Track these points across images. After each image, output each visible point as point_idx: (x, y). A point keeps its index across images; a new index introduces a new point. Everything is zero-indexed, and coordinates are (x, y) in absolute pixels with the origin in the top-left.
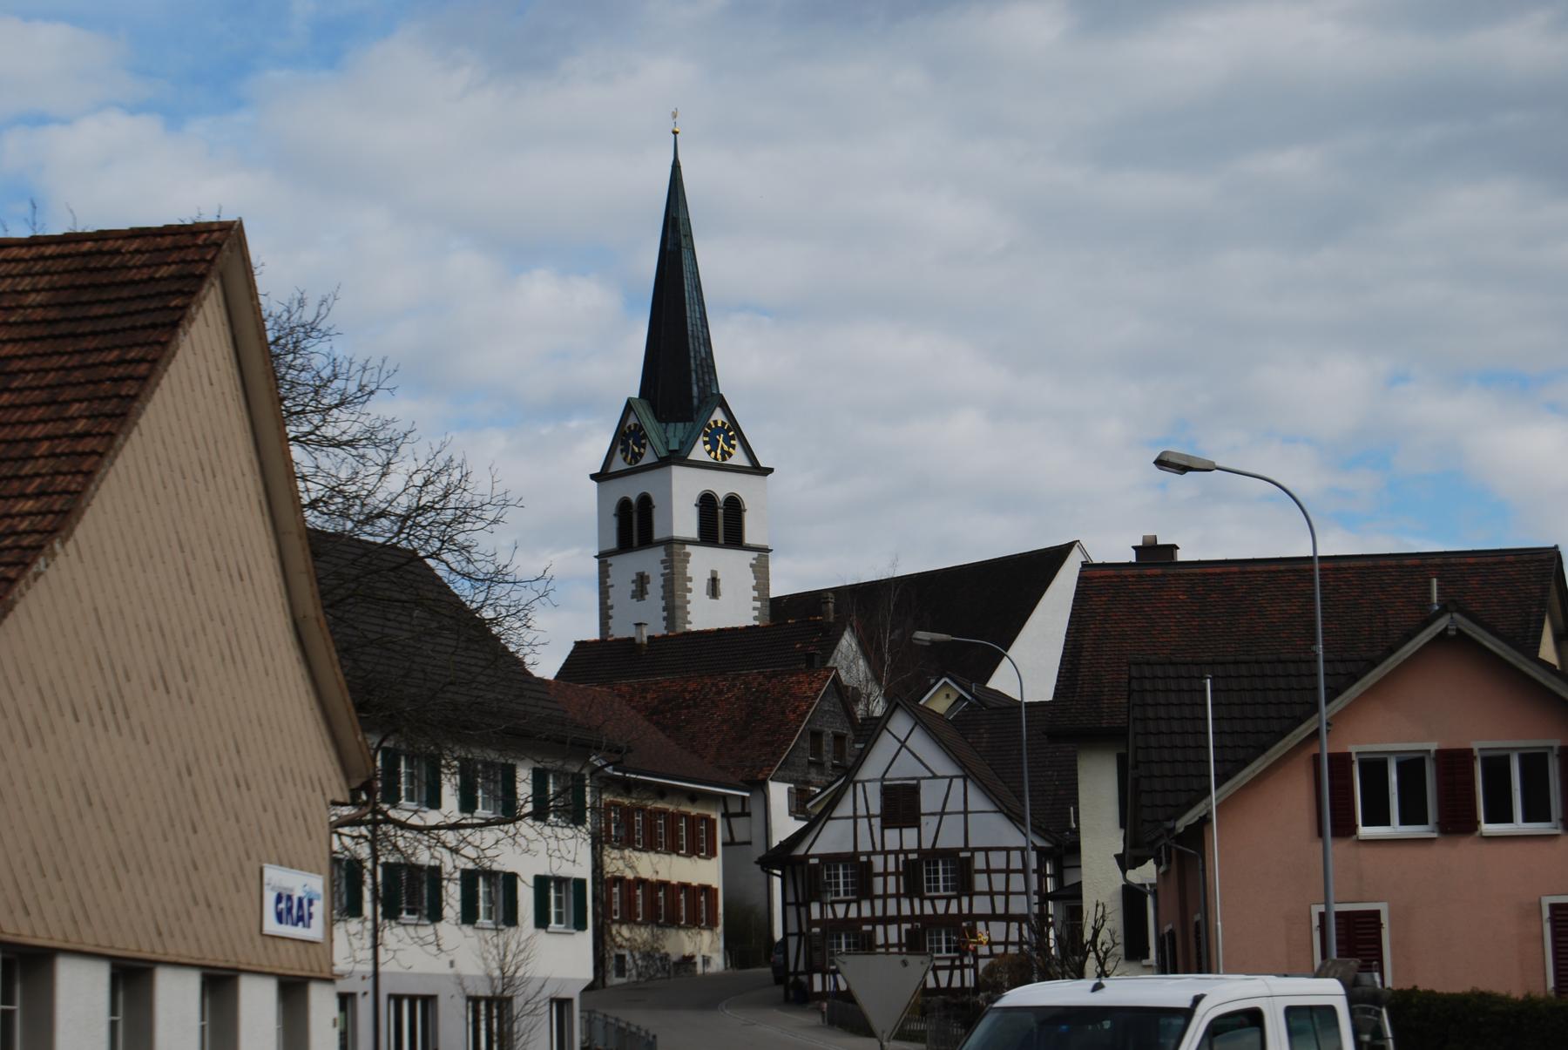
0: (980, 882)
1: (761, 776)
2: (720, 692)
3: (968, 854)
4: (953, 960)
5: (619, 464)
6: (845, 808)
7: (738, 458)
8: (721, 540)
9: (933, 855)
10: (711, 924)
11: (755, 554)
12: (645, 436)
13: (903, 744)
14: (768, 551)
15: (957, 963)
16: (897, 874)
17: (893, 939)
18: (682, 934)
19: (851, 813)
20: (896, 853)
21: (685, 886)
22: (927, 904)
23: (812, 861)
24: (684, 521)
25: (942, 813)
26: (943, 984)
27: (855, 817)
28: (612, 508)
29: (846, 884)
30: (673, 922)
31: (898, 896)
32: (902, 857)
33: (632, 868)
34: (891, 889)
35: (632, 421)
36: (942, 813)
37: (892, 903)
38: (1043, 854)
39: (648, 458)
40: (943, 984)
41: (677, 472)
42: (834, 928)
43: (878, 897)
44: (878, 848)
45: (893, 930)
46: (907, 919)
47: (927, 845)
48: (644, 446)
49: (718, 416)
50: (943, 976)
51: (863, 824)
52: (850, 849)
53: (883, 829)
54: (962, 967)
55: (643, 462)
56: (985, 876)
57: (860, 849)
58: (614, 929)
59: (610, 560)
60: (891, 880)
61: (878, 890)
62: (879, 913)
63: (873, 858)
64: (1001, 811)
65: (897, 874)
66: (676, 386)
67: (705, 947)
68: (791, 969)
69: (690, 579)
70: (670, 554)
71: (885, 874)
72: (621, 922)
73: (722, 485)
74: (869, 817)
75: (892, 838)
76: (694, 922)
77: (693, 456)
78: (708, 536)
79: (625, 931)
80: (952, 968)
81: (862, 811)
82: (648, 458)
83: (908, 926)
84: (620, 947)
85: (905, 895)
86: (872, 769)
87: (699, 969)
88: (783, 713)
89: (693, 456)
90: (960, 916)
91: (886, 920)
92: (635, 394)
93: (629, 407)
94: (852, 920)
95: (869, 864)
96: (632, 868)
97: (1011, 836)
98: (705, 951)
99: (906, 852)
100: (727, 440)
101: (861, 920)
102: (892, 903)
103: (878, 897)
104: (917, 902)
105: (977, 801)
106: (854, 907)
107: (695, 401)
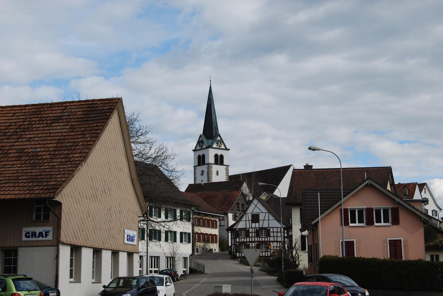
0: (272, 234)
2: (218, 195)
6: (244, 219)
7: (223, 147)
9: (262, 229)
10: (216, 242)
13: (256, 206)
14: (228, 166)
16: (254, 232)
17: (254, 246)
18: (210, 244)
20: (254, 228)
21: (211, 234)
22: (261, 239)
24: (211, 160)
25: (264, 220)
26: (264, 255)
27: (246, 221)
28: (197, 157)
30: (208, 242)
31: (255, 237)
34: (253, 236)
35: (201, 139)
36: (264, 220)
37: (253, 238)
38: (284, 229)
39: (204, 147)
41: (210, 149)
42: (242, 243)
45: (253, 244)
47: (261, 226)
49: (219, 138)
50: (264, 253)
51: (248, 222)
54: (268, 252)
58: (196, 243)
60: (253, 234)
61: (251, 236)
62: (251, 240)
65: (254, 232)
67: (215, 247)
70: (208, 166)
71: (252, 232)
72: (198, 242)
73: (219, 152)
74: (249, 221)
76: (213, 242)
78: (216, 163)
79: (198, 243)
80: (265, 252)
81: (247, 219)
82: (204, 147)
86: (250, 211)
87: (214, 252)
91: (252, 242)
93: (200, 136)
95: (249, 230)
99: (256, 228)
100: (221, 143)
101: (247, 242)
102: (253, 238)
105: (271, 217)
106: (245, 239)
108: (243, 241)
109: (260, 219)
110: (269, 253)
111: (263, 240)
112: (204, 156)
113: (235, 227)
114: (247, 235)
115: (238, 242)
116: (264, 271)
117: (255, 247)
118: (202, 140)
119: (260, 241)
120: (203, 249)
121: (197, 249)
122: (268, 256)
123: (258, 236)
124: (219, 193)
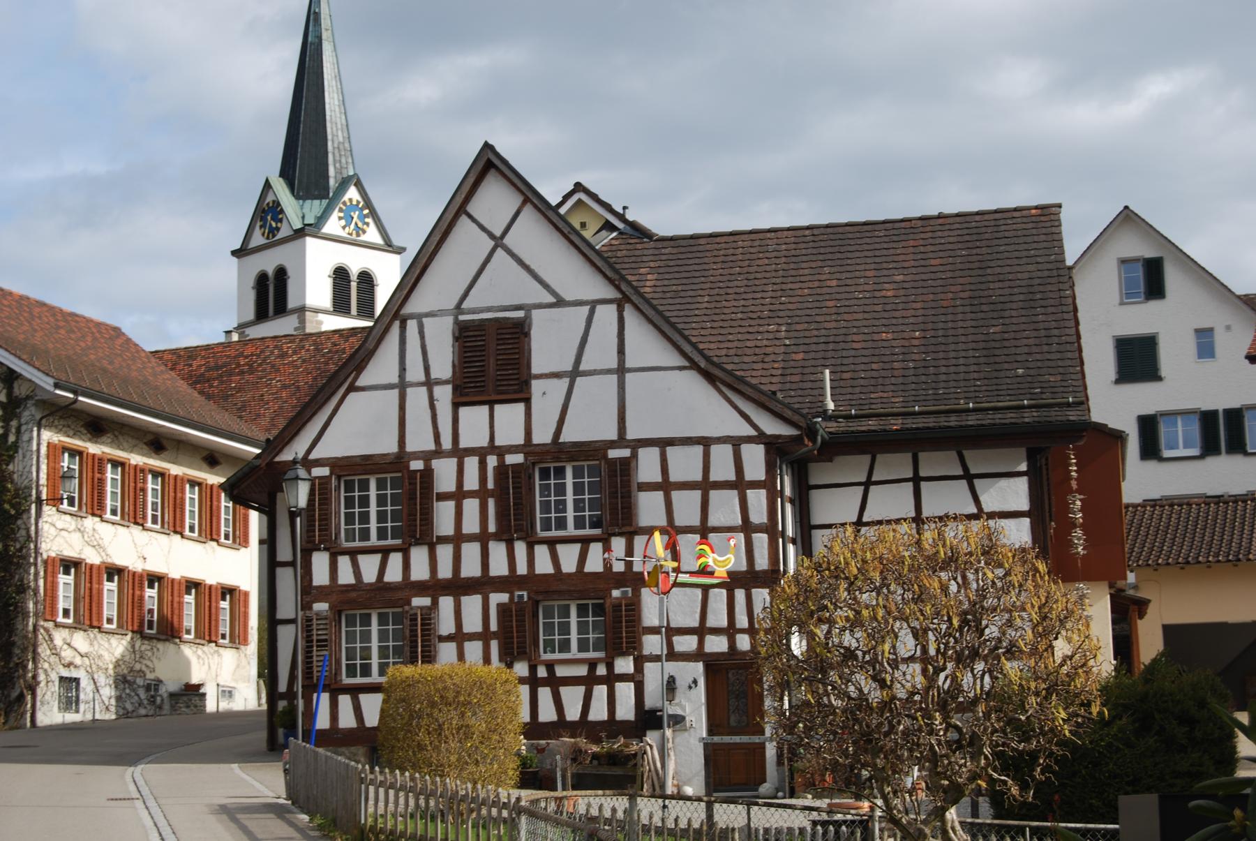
0: (649, 508)
2: (283, 355)
3: (626, 453)
4: (592, 665)
5: (258, 239)
7: (372, 235)
8: (354, 311)
9: (558, 454)
10: (237, 639)
12: (282, 211)
13: (499, 242)
15: (601, 670)
16: (482, 494)
17: (473, 623)
18: (187, 650)
19: (395, 380)
20: (481, 453)
21: (192, 585)
22: (542, 552)
25: (575, 373)
26: (573, 714)
27: (402, 386)
28: (251, 281)
29: (381, 517)
30: (168, 631)
31: (483, 538)
32: (492, 461)
33: (98, 547)
34: (471, 525)
35: (270, 198)
36: (575, 373)
37: (471, 552)
38: (776, 449)
40: (573, 714)
41: (310, 242)
42: (354, 602)
44: (447, 444)
45: (472, 604)
47: (542, 436)
48: (281, 221)
50: (572, 698)
51: (418, 398)
52: (391, 447)
53: (456, 405)
54: (611, 679)
55: (280, 236)
56: (659, 496)
57: (410, 448)
58: (59, 637)
60: (471, 506)
62: (445, 572)
63: (436, 464)
64: (694, 366)
65: (482, 494)
67: (228, 676)
71: (459, 495)
72: (75, 627)
73: (356, 261)
74: (429, 383)
75: (474, 425)
76: (207, 633)
79: (80, 640)
80: (589, 681)
81: (415, 372)
82: (284, 232)
83: (504, 597)
85: (497, 537)
87: (211, 706)
90: (608, 578)
91: (459, 587)
95: (428, 474)
96: (98, 547)
97: (714, 413)
98: (226, 680)
99: (501, 452)
101: (411, 587)
102: (471, 552)
103: (443, 540)
104: (520, 548)
105: (644, 345)
106: (396, 560)
108: (370, 576)
109: (535, 370)
110: (625, 691)
111: (569, 566)
112: (281, 273)
114: (414, 528)
117: (484, 636)
118: (277, 204)
119: (531, 580)
120: (123, 681)
121: (70, 684)
122: (612, 727)
123: (515, 522)
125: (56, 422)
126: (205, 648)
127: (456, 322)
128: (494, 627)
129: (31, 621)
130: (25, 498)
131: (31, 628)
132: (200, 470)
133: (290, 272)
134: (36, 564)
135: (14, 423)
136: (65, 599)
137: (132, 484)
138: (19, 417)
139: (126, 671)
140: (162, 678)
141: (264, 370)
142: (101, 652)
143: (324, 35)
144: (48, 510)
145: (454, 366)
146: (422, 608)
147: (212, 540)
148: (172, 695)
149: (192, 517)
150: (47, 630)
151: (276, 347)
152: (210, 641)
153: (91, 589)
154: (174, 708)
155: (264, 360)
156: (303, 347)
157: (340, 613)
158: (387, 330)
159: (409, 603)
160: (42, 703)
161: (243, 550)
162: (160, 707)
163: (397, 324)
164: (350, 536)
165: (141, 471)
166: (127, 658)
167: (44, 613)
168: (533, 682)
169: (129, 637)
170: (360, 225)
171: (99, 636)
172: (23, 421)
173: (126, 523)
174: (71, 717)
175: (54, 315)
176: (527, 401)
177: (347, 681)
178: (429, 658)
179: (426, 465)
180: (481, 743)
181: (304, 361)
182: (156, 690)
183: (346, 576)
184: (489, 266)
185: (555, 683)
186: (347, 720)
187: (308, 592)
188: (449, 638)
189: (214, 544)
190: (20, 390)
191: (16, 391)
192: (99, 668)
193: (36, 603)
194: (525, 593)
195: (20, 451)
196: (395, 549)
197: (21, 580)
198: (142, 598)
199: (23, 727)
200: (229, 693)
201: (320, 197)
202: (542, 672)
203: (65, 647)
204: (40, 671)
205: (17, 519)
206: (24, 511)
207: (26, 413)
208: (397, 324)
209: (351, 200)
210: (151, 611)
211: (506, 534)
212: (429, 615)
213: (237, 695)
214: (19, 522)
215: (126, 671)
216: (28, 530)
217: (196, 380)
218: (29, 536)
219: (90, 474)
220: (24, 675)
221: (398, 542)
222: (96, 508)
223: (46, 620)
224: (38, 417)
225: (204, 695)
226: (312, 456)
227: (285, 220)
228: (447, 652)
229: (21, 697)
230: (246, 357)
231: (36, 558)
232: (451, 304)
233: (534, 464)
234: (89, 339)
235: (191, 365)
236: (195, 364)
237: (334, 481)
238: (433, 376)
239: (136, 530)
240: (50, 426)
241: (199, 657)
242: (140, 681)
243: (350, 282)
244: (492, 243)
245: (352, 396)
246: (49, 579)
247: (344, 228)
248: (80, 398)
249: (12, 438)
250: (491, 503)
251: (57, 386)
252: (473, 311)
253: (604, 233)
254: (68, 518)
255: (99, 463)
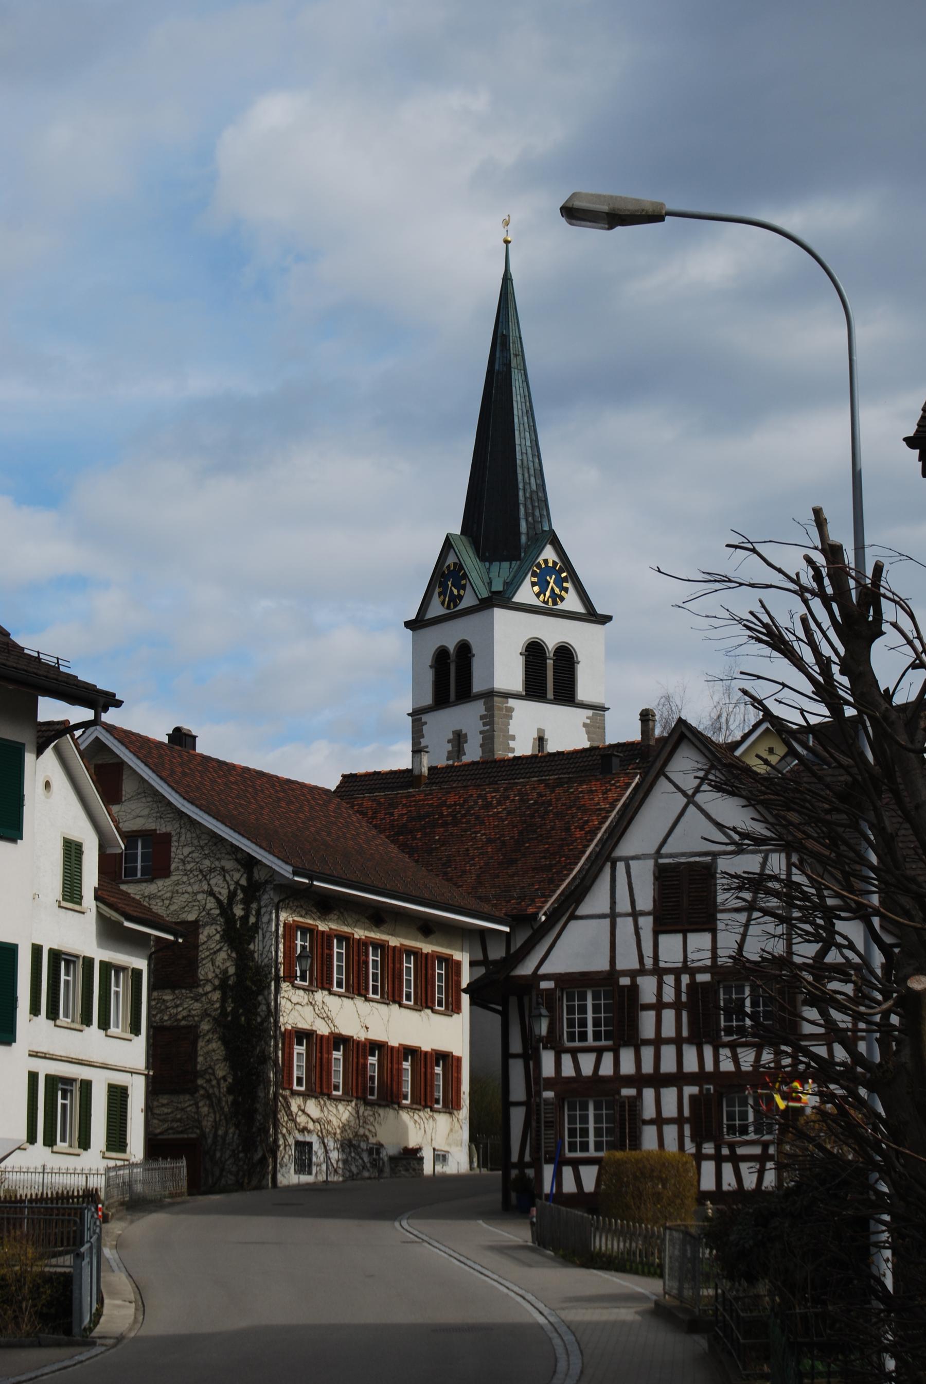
1: (531, 910)
2: (488, 806)
4: (765, 1146)
5: (436, 609)
6: (597, 901)
7: (571, 602)
8: (550, 695)
9: (741, 970)
10: (451, 1105)
11: (590, 713)
12: (465, 576)
14: (603, 709)
16: (677, 1006)
17: (670, 1110)
18: (405, 1116)
19: (607, 910)
20: (677, 973)
21: (410, 1052)
23: (544, 985)
24: (507, 671)
27: (613, 916)
28: (428, 659)
29: (596, 1023)
30: (390, 1098)
31: (678, 1042)
32: (685, 979)
33: (327, 1018)
34: (668, 1031)
35: (451, 560)
39: (469, 600)
41: (499, 614)
42: (577, 1090)
43: (647, 1042)
44: (649, 963)
45: (669, 1095)
46: (692, 1079)
48: (464, 587)
49: (549, 554)
51: (625, 926)
52: (606, 967)
53: (656, 933)
55: (463, 605)
57: (619, 967)
58: (295, 1103)
59: (425, 718)
60: (669, 1016)
61: (647, 1028)
63: (640, 980)
65: (677, 1006)
66: (505, 519)
67: (442, 1139)
68: (515, 1158)
69: (513, 738)
70: (490, 708)
71: (659, 1006)
72: (306, 1095)
73: (552, 632)
74: (635, 914)
75: (671, 948)
76: (424, 1100)
77: (519, 598)
78: (534, 690)
79: (312, 1107)
81: (623, 905)
82: (469, 600)
83: (694, 1090)
84: (304, 1130)
85: (690, 1041)
86: (641, 839)
87: (428, 1168)
88: (568, 830)
89: (519, 598)
91: (659, 1080)
92: (457, 530)
93: (448, 544)
94: (605, 1079)
95: (634, 989)
96: (327, 1018)
98: (441, 1144)
99: (693, 972)
100: (559, 582)
101: (619, 1080)
103: (647, 1042)
104: (708, 1051)
106: (608, 1058)
107: (523, 539)
108: (750, 1182)
112: (464, 649)
113: (526, 969)
114: (622, 1029)
115: (550, 1083)
116: (693, 1326)
117: (679, 1121)
118: (459, 566)
119: (717, 1076)
120: (349, 1145)
121: (304, 1148)
123: (702, 1032)
124: (492, 796)
125: (291, 904)
126: (421, 1114)
127: (657, 865)
128: (686, 1113)
129: (272, 1090)
130: (266, 976)
131: (271, 1096)
132: (416, 940)
133: (475, 650)
134: (275, 1037)
135: (254, 905)
136: (298, 1069)
137: (356, 958)
138: (259, 901)
139: (351, 1136)
140: (383, 1142)
141: (468, 822)
142: (330, 1118)
143: (513, 364)
144: (285, 986)
145: (654, 901)
146: (628, 1097)
147: (427, 1007)
148: (392, 1159)
149: (409, 986)
150: (285, 1098)
151: (480, 796)
152: (426, 1106)
153: (321, 1059)
154: (393, 1171)
155: (468, 811)
156: (508, 797)
157: (563, 1100)
158: (600, 870)
159: (619, 1093)
160: (281, 1166)
161: (455, 1016)
162: (381, 1171)
163: (609, 864)
164: (571, 1038)
165: (364, 944)
166: (352, 1124)
167: (282, 1082)
168: (719, 1159)
169: (353, 1104)
170: (557, 591)
171: (328, 1103)
172: (262, 903)
173: (351, 995)
174: (305, 1179)
175: (273, 786)
176: (714, 931)
177: (569, 1155)
178: (636, 1142)
179: (632, 981)
180: (669, 1205)
181: (509, 813)
182: (378, 1153)
183: (568, 1070)
184: (683, 820)
185: (736, 1160)
186: (569, 1186)
187: (534, 1080)
188: (651, 1122)
189: (429, 1011)
190: (259, 875)
191: (256, 876)
192: (328, 1132)
193: (275, 1074)
194: (712, 1087)
195: (260, 932)
196: (607, 1049)
197: (263, 1051)
198: (365, 1065)
199: (266, 1187)
200: (440, 1157)
201: (510, 559)
202: (725, 1151)
203: (300, 1113)
204: (280, 1136)
205: (258, 995)
206: (264, 988)
207: (266, 897)
208: (609, 864)
209: (546, 561)
210: (372, 1078)
211: (697, 1040)
212: (636, 1103)
213: (450, 1159)
214: (260, 998)
215: (351, 1136)
216: (269, 1005)
217: (399, 834)
218: (269, 1010)
219: (320, 950)
220: (267, 1139)
221: (610, 1043)
222: (324, 983)
223: (284, 1089)
224: (276, 900)
225: (422, 1159)
226: (542, 971)
227: (468, 587)
228: (649, 1136)
229: (263, 1160)
230: (450, 807)
231: (275, 1032)
232: (652, 850)
233: (719, 982)
234: (306, 808)
235: (392, 814)
236: (396, 813)
237: (558, 993)
238: (638, 909)
239: (359, 1001)
240: (286, 908)
241: (415, 1122)
242: (363, 1145)
243: (545, 659)
244: (685, 800)
245: (573, 924)
246: (287, 1050)
247: (538, 595)
248: (315, 883)
249: (252, 920)
250: (685, 1014)
251: (295, 873)
252: (671, 856)
253: (789, 759)
254: (301, 992)
255: (325, 940)
